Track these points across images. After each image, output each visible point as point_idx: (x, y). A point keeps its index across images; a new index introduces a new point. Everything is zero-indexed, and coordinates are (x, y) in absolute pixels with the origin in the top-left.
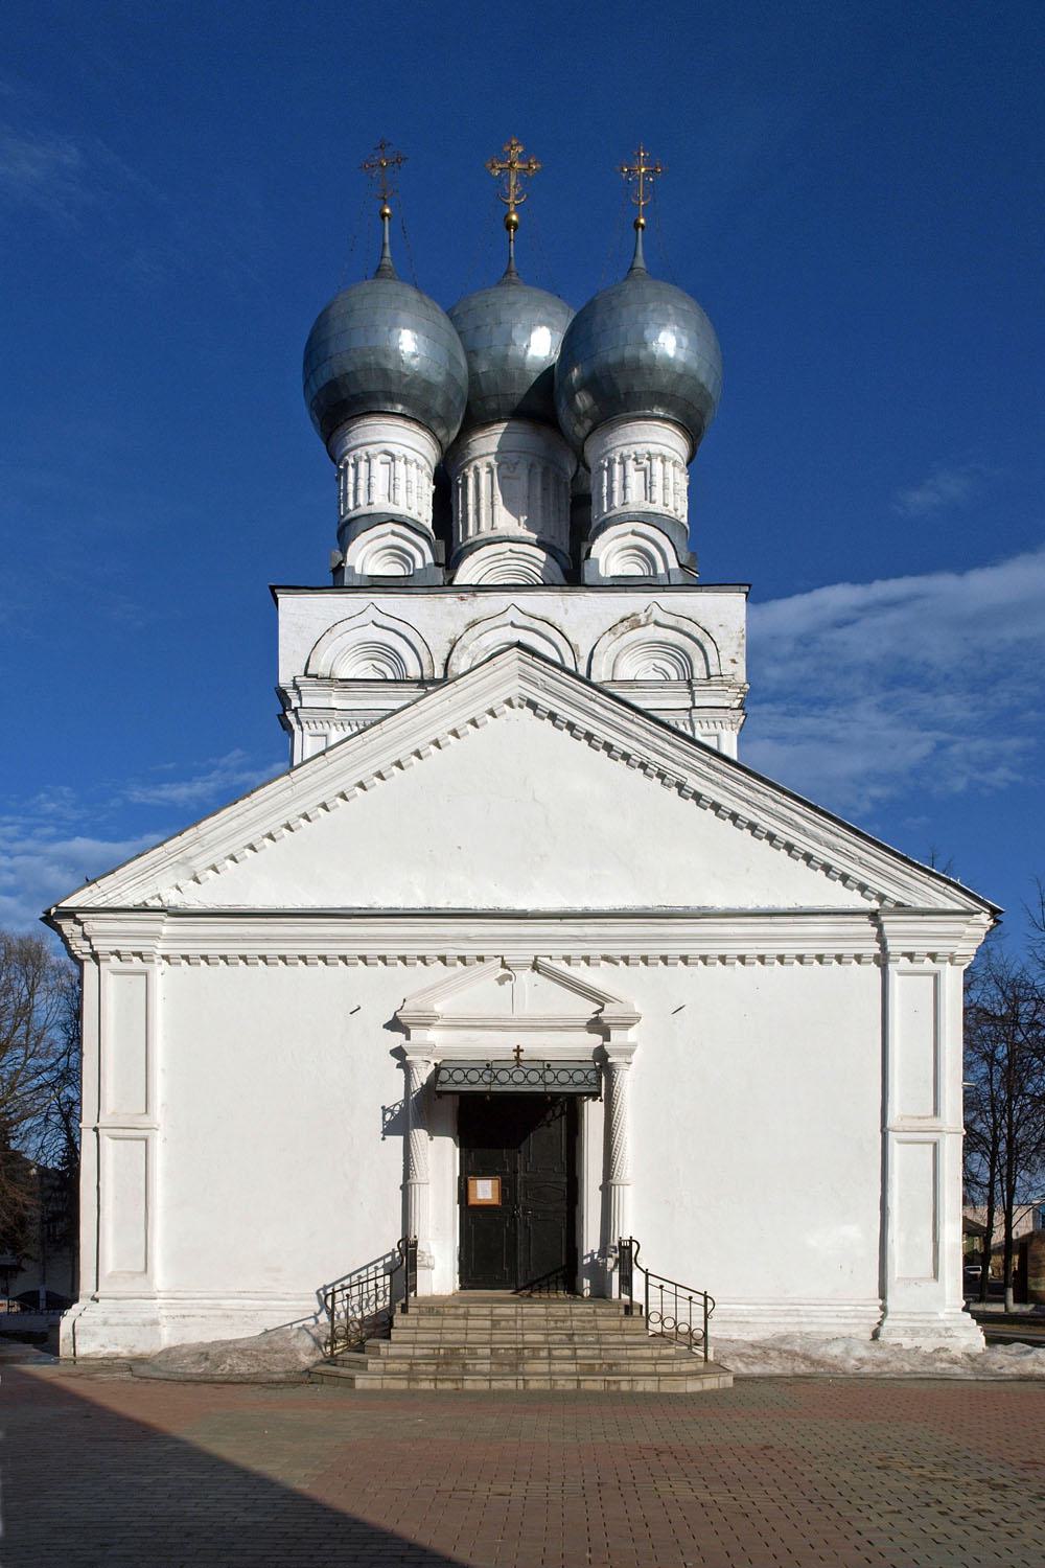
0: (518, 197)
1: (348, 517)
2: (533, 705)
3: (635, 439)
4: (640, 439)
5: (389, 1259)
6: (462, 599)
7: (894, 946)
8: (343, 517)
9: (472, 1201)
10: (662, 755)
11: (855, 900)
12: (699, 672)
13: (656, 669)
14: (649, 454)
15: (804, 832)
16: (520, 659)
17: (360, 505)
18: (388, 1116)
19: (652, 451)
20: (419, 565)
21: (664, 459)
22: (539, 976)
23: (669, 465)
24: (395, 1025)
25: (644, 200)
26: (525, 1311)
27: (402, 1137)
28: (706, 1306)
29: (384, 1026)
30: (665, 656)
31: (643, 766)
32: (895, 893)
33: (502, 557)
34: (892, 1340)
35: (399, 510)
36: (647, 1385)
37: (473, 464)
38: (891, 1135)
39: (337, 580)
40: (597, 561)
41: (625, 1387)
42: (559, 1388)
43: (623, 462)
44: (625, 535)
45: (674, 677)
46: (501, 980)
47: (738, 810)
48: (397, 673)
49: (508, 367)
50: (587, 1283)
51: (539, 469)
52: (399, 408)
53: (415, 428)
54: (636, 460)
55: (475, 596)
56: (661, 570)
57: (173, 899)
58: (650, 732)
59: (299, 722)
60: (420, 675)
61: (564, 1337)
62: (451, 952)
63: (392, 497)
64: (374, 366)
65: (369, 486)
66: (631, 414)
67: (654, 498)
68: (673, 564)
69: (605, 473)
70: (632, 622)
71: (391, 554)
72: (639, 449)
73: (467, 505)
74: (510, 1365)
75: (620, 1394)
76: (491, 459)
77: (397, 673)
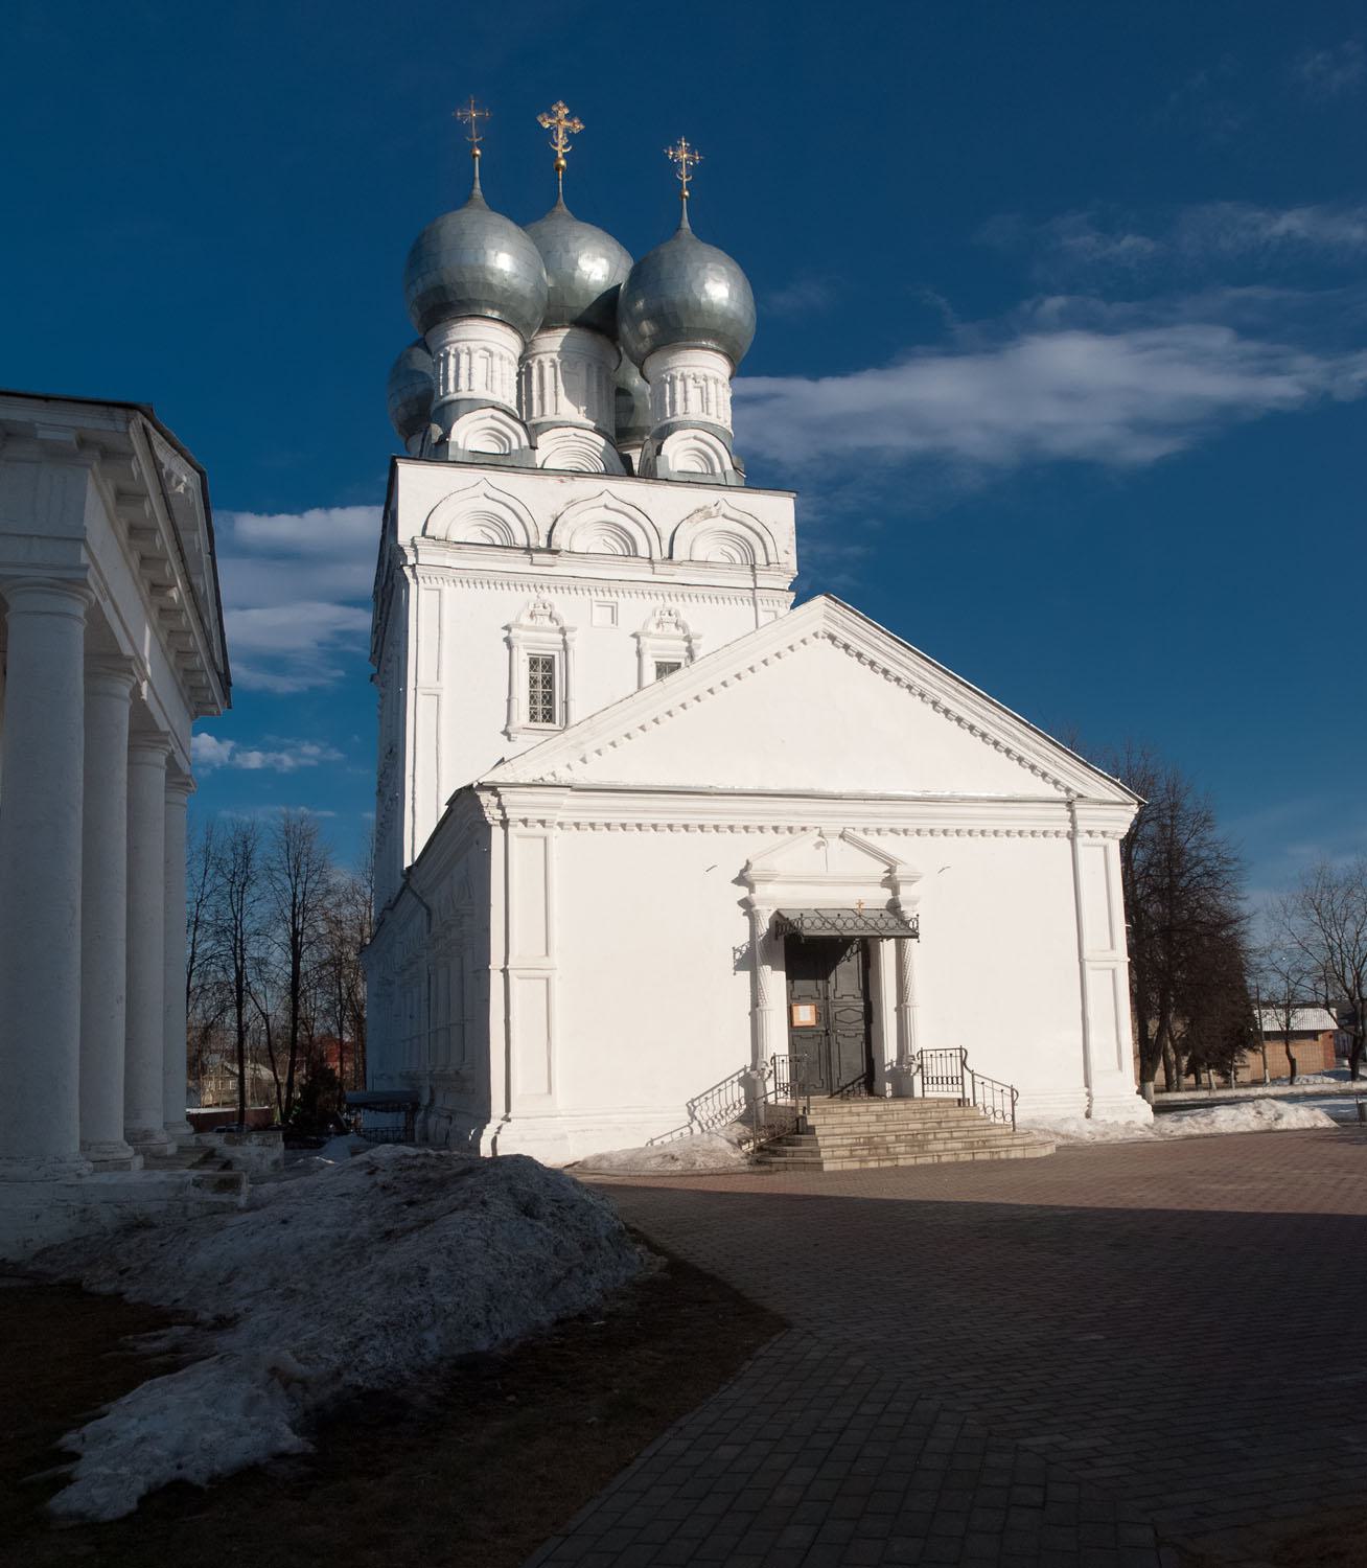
0: (564, 147)
1: (448, 398)
2: (832, 638)
3: (692, 363)
5: (742, 1074)
6: (562, 481)
7: (1082, 826)
8: (442, 397)
9: (796, 1024)
10: (924, 680)
11: (1050, 791)
12: (760, 560)
13: (723, 553)
14: (705, 376)
15: (1019, 741)
16: (826, 605)
17: (461, 390)
18: (738, 956)
19: (708, 374)
20: (515, 446)
21: (716, 381)
22: (845, 844)
23: (719, 385)
24: (741, 880)
25: (687, 177)
26: (890, 1107)
27: (748, 973)
28: (1012, 1096)
29: (733, 882)
30: (731, 543)
31: (910, 687)
32: (1078, 788)
34: (1100, 1118)
35: (496, 398)
36: (1016, 1154)
37: (538, 357)
38: (1087, 965)
39: (437, 453)
40: (667, 457)
41: (1003, 1156)
42: (961, 1159)
43: (684, 379)
44: (688, 438)
45: (738, 561)
46: (818, 845)
47: (974, 723)
48: (504, 540)
49: (567, 282)
50: (888, 1086)
51: (595, 369)
52: (496, 315)
53: (509, 330)
54: (694, 379)
55: (573, 479)
56: (718, 470)
57: (565, 776)
58: (917, 664)
59: (415, 576)
60: (526, 543)
61: (935, 1124)
62: (783, 824)
63: (489, 386)
64: (481, 280)
65: (470, 375)
66: (691, 343)
67: (710, 411)
68: (729, 467)
69: (667, 386)
70: (703, 512)
71: (488, 434)
72: (697, 371)
73: (531, 391)
74: (918, 1146)
75: (1001, 1161)
76: (555, 356)
77: (504, 540)
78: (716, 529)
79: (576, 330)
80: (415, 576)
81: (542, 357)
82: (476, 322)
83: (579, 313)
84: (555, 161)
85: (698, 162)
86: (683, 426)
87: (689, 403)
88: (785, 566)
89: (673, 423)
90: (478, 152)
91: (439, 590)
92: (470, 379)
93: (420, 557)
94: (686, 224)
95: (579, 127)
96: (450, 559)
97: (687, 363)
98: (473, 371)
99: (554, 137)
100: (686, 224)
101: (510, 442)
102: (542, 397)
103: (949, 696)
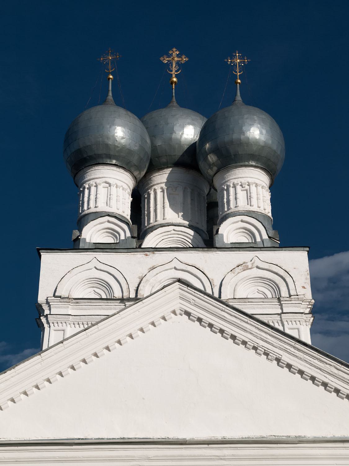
0: (176, 71)
2: (188, 314)
4: (243, 176)
6: (146, 255)
8: (81, 213)
10: (266, 342)
14: (249, 183)
16: (180, 289)
17: (91, 208)
19: (250, 182)
30: (264, 285)
31: (255, 348)
33: (169, 233)
37: (153, 187)
40: (222, 235)
43: (235, 187)
45: (270, 296)
47: (315, 375)
51: (189, 190)
52: (114, 162)
53: (122, 170)
54: (241, 185)
56: (258, 239)
59: (48, 323)
60: (121, 296)
65: (96, 198)
66: (238, 164)
68: (265, 237)
69: (225, 192)
70: (243, 266)
72: (243, 180)
73: (150, 208)
76: (163, 185)
78: (252, 276)
79: (176, 169)
80: (48, 323)
81: (156, 187)
82: (100, 167)
83: (177, 158)
84: (170, 79)
85: (246, 63)
86: (234, 214)
87: (238, 200)
88: (302, 296)
89: (229, 214)
90: (111, 77)
91: (64, 330)
92: (96, 200)
93: (52, 310)
94: (239, 98)
95: (185, 59)
96: (71, 310)
97: (236, 176)
98: (98, 195)
99: (170, 67)
100: (239, 98)
101: (119, 235)
102: (155, 211)
103: (290, 353)
